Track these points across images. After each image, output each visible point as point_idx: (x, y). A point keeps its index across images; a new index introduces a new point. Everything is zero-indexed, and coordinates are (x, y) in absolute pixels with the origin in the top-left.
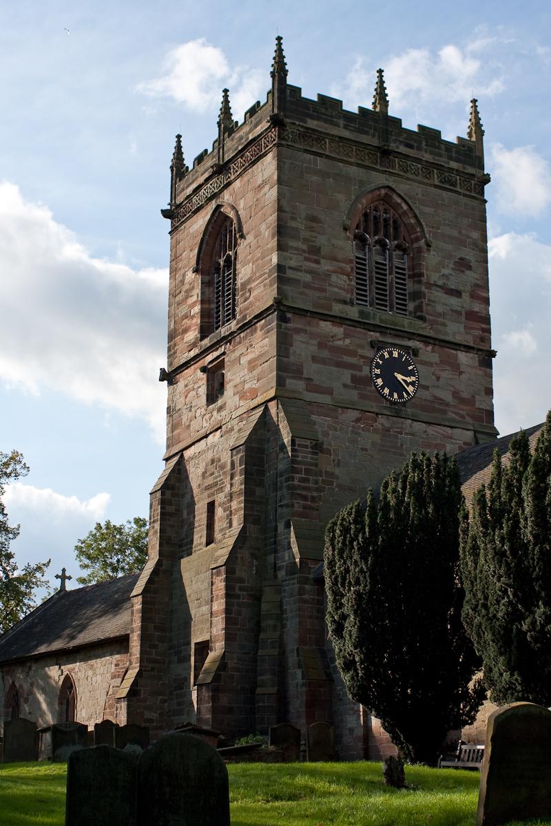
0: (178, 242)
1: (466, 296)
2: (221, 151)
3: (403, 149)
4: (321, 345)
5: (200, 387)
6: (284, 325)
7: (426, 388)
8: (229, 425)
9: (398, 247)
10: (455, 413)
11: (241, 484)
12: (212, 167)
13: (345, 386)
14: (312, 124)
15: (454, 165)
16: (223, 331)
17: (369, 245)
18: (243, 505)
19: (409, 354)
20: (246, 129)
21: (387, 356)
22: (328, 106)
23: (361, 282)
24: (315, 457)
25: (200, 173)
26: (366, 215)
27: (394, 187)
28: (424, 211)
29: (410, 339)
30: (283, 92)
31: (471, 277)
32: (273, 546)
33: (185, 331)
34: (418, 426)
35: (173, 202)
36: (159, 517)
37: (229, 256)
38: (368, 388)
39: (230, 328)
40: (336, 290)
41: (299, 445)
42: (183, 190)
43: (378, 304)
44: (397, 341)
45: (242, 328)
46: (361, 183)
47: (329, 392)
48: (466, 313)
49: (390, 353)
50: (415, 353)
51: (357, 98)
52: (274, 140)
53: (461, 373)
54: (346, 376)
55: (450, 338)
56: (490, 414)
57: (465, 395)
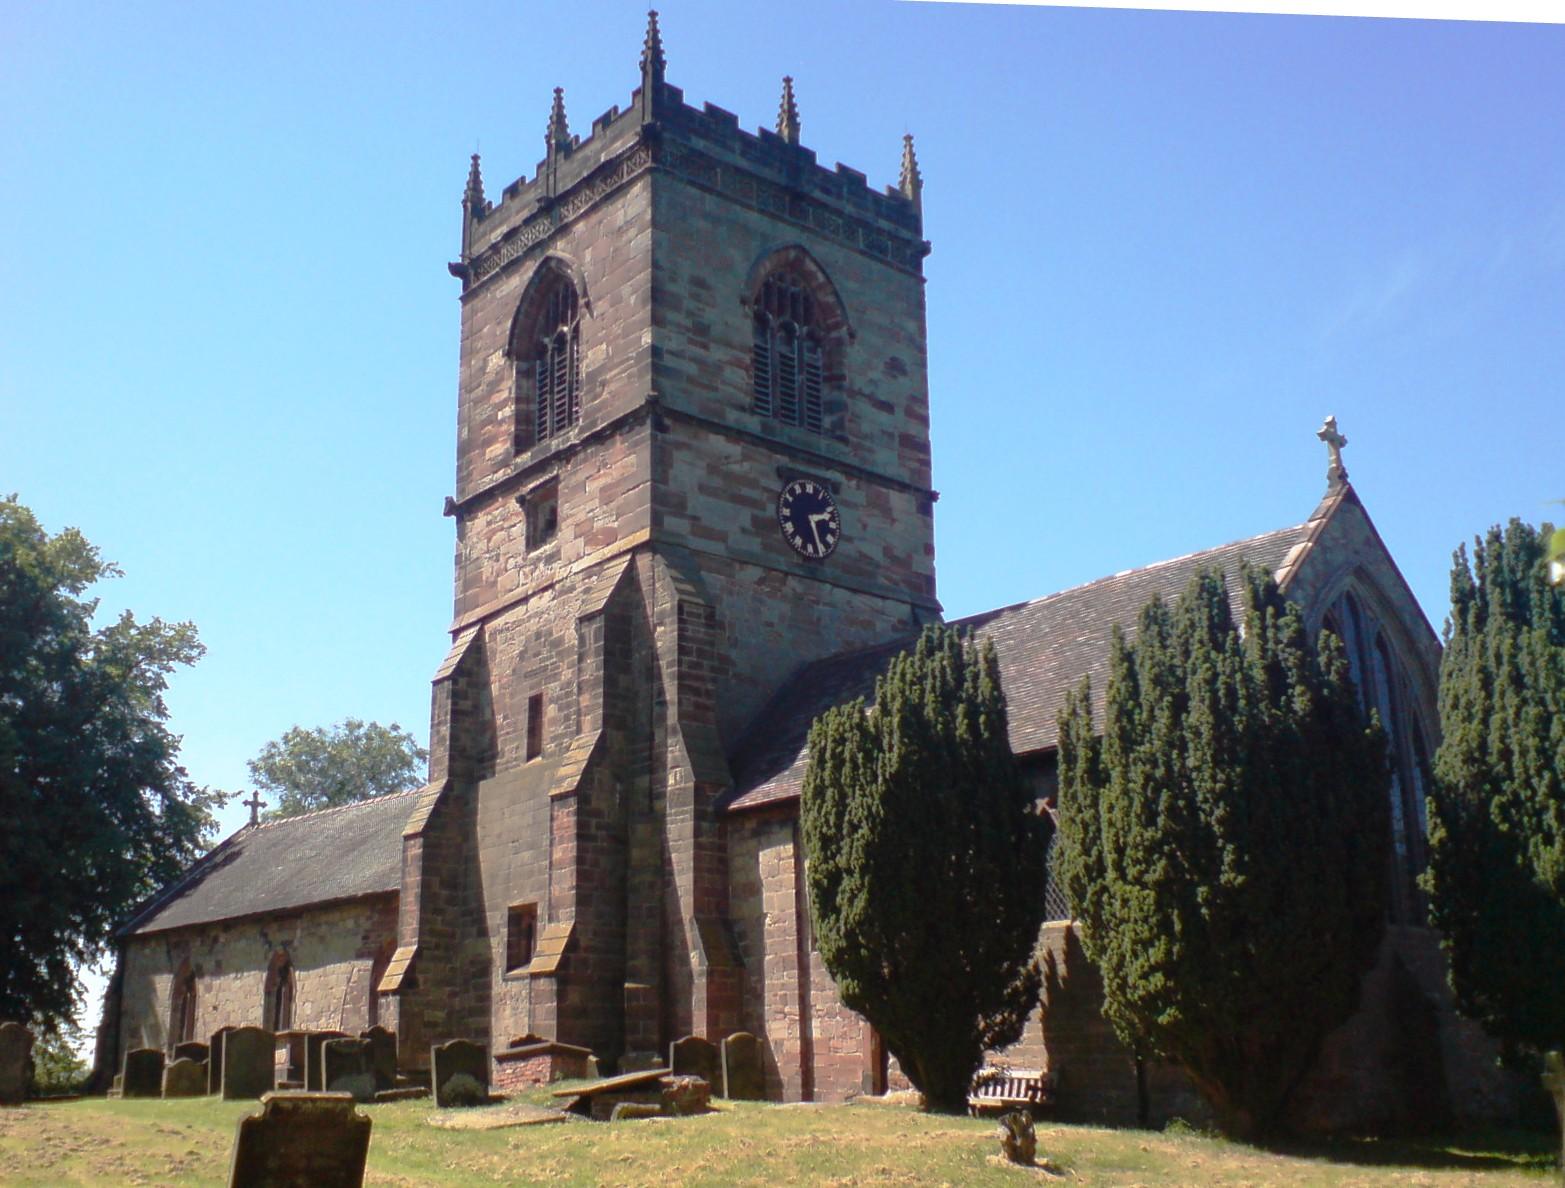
0: (474, 312)
1: (899, 413)
2: (551, 178)
3: (817, 194)
4: (713, 469)
5: (514, 526)
6: (660, 436)
7: (849, 539)
8: (568, 583)
9: (811, 336)
10: (887, 578)
11: (598, 669)
12: (539, 201)
13: (744, 530)
14: (700, 144)
15: (884, 224)
16: (555, 444)
17: (772, 329)
18: (601, 700)
19: (826, 489)
20: (596, 145)
21: (798, 490)
22: (718, 121)
23: (761, 381)
24: (711, 631)
25: (514, 210)
26: (767, 285)
27: (807, 247)
28: (848, 285)
29: (828, 469)
30: (660, 96)
31: (904, 384)
32: (647, 764)
33: (489, 442)
34: (841, 595)
35: (467, 252)
36: (449, 717)
37: (562, 335)
38: (775, 536)
39: (568, 439)
40: (731, 390)
41: (690, 614)
42: (484, 234)
43: (783, 415)
44: (813, 471)
45: (586, 443)
46: (764, 237)
47: (722, 537)
48: (900, 436)
49: (803, 487)
50: (836, 488)
51: (756, 117)
52: (645, 162)
53: (894, 521)
54: (745, 516)
55: (880, 470)
56: (930, 581)
57: (899, 552)
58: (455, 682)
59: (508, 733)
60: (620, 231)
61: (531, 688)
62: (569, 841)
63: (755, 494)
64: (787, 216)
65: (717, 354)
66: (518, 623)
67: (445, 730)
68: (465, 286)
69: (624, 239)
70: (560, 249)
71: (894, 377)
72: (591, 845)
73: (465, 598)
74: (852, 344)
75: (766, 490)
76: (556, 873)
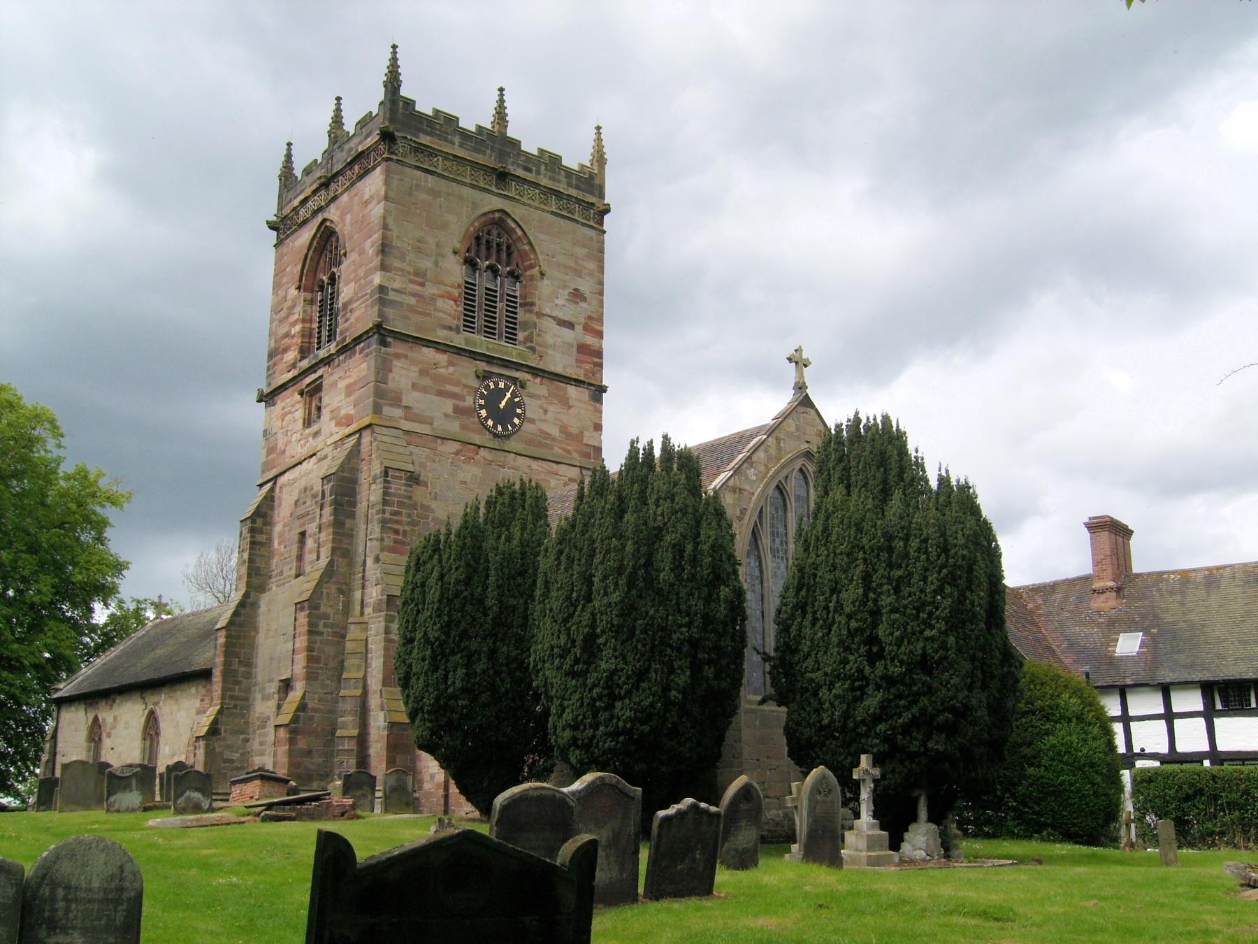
3: (520, 172)
4: (423, 372)
7: (532, 421)
11: (330, 515)
13: (446, 415)
14: (425, 140)
19: (515, 384)
21: (492, 386)
25: (308, 184)
27: (508, 211)
33: (285, 350)
43: (485, 332)
45: (339, 352)
47: (429, 422)
49: (496, 384)
51: (475, 117)
53: (570, 407)
54: (448, 406)
57: (574, 430)
58: (253, 522)
59: (286, 558)
60: (367, 203)
61: (300, 527)
62: (304, 635)
63: (457, 390)
64: (493, 189)
65: (430, 290)
66: (295, 481)
67: (246, 556)
68: (278, 237)
69: (368, 209)
70: (333, 213)
71: (577, 303)
72: (318, 638)
73: (267, 461)
74: (542, 279)
75: (465, 386)
76: (296, 657)
